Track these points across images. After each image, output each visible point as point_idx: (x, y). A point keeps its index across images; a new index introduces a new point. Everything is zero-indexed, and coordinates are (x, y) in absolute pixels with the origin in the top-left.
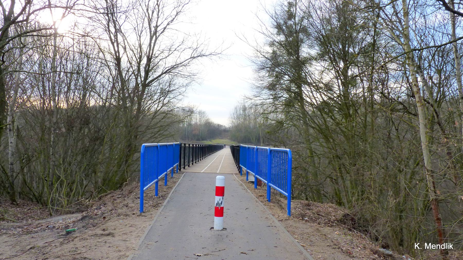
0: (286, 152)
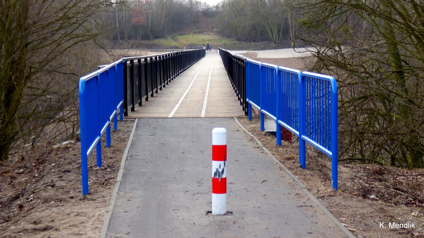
0: (328, 82)
